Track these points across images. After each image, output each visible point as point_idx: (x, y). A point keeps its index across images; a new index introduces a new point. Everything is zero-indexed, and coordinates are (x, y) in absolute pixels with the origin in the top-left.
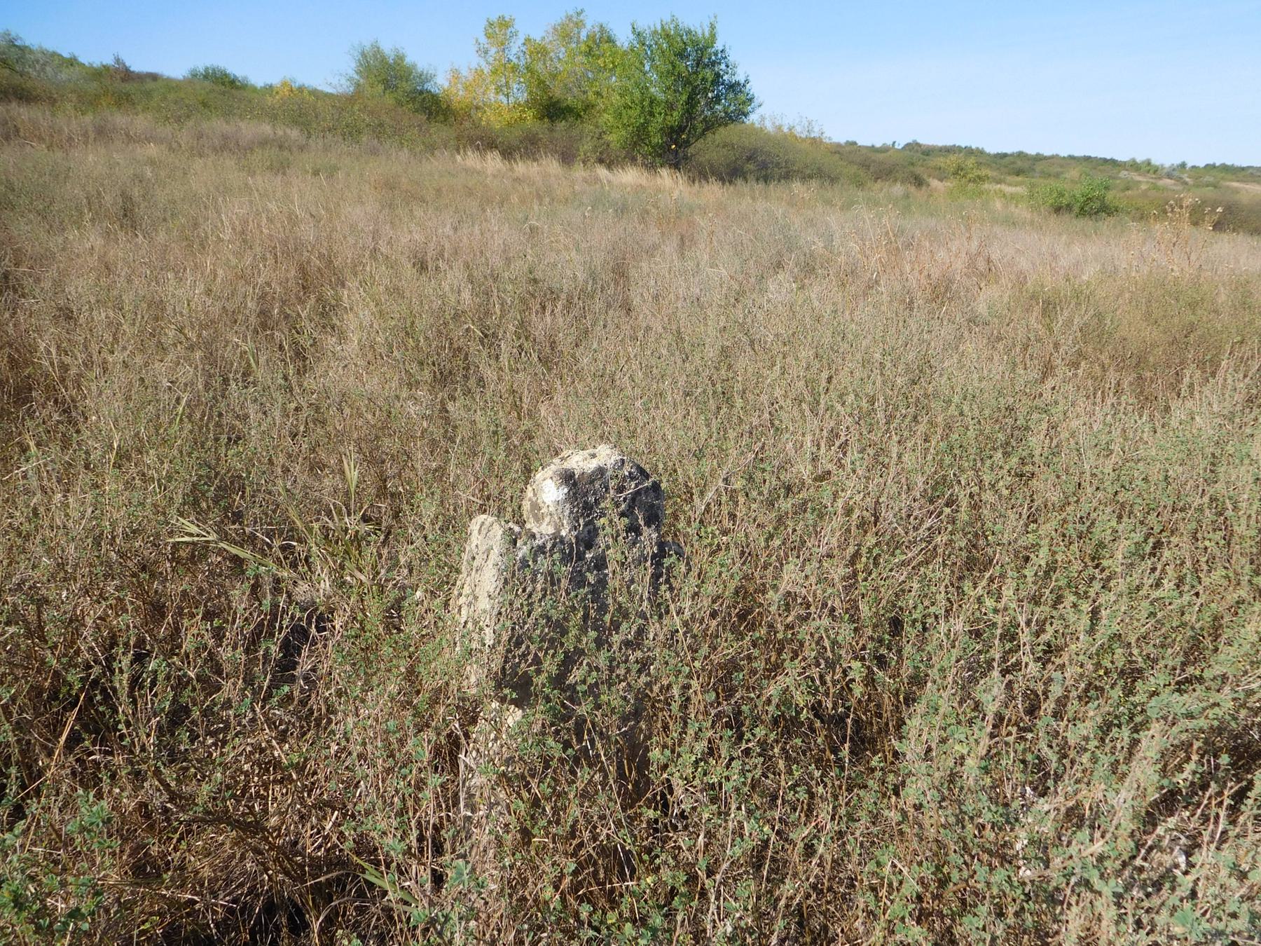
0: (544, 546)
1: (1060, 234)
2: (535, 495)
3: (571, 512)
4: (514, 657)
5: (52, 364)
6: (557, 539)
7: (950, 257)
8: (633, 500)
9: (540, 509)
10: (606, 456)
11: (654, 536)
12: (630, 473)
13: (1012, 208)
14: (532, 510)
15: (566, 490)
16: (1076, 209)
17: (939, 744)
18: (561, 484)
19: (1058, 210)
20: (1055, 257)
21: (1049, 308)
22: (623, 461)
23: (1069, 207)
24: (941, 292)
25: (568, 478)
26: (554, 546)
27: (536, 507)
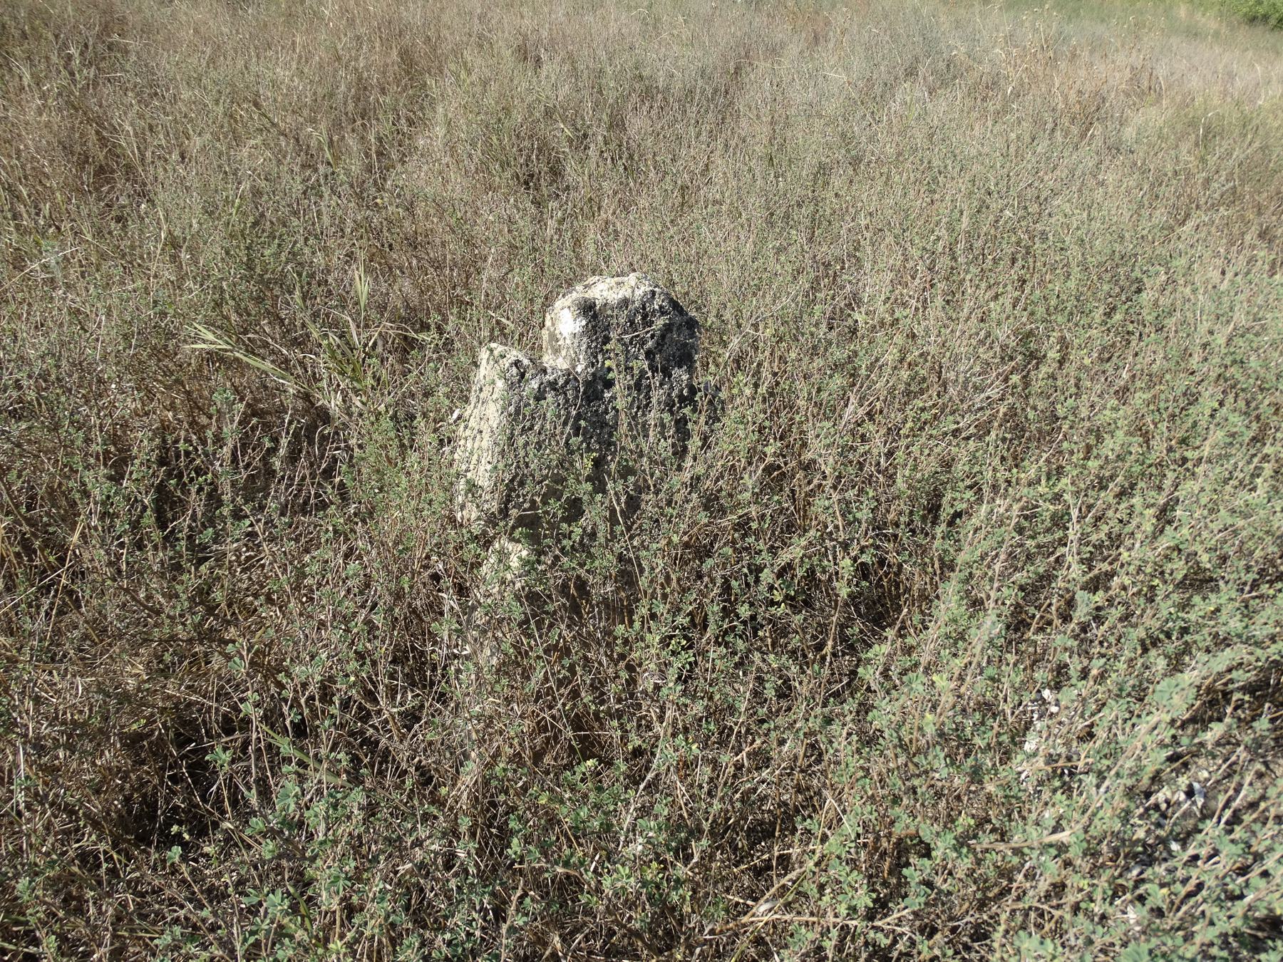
0: (555, 382)
1: (1247, 49)
2: (553, 325)
3: (589, 347)
4: (518, 496)
5: (133, 152)
6: (569, 376)
7: (1111, 73)
8: (663, 337)
9: (557, 340)
10: (632, 287)
11: (685, 377)
12: (661, 307)
13: (1198, 16)
14: (550, 341)
15: (584, 323)
16: (1273, 21)
17: (935, 671)
18: (579, 315)
19: (1252, 20)
20: (1231, 76)
21: (1210, 135)
22: (653, 293)
23: (1266, 18)
24: (1090, 113)
25: (588, 309)
26: (567, 382)
27: (554, 338)
